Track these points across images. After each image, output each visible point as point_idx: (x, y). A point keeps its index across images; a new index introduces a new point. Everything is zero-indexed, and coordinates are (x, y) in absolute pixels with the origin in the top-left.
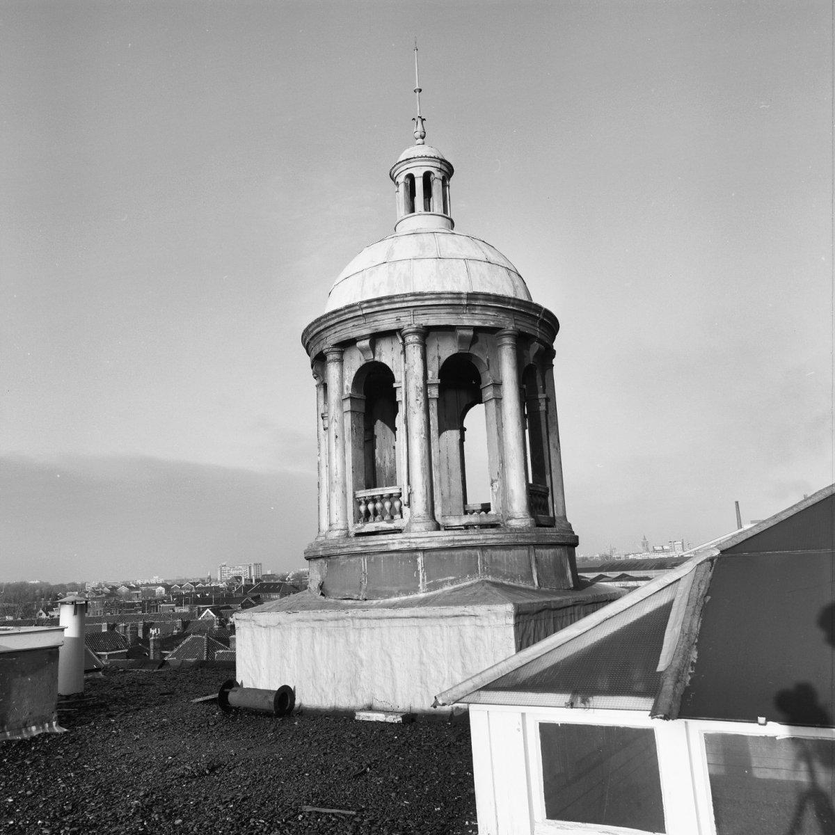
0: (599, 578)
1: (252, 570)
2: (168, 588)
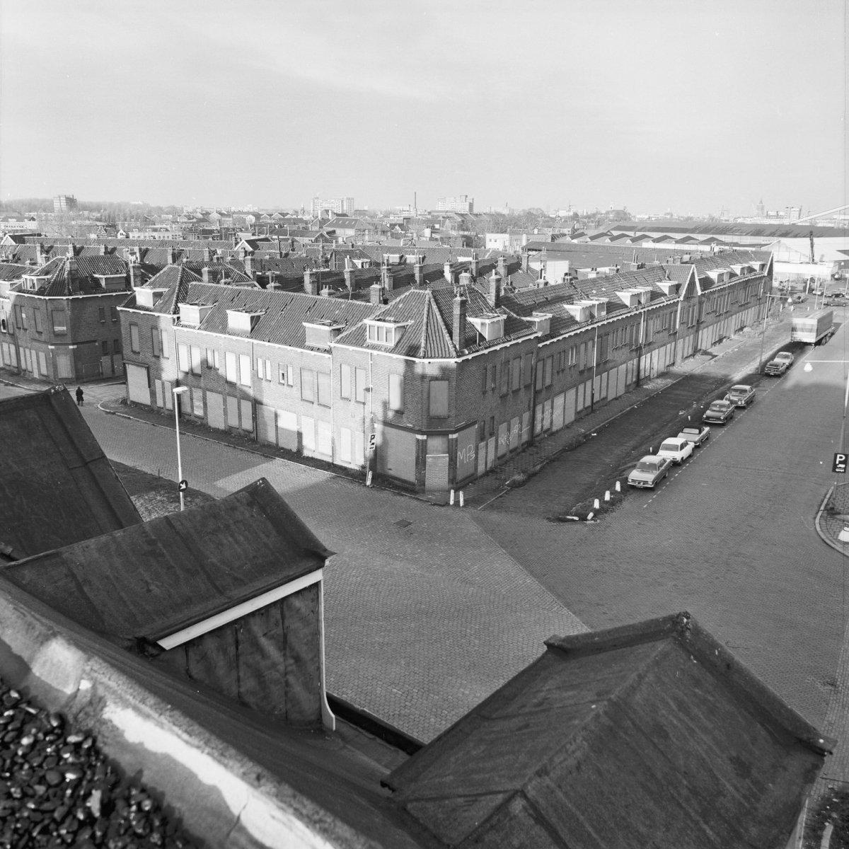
0: (644, 237)
1: (345, 204)
2: (258, 216)
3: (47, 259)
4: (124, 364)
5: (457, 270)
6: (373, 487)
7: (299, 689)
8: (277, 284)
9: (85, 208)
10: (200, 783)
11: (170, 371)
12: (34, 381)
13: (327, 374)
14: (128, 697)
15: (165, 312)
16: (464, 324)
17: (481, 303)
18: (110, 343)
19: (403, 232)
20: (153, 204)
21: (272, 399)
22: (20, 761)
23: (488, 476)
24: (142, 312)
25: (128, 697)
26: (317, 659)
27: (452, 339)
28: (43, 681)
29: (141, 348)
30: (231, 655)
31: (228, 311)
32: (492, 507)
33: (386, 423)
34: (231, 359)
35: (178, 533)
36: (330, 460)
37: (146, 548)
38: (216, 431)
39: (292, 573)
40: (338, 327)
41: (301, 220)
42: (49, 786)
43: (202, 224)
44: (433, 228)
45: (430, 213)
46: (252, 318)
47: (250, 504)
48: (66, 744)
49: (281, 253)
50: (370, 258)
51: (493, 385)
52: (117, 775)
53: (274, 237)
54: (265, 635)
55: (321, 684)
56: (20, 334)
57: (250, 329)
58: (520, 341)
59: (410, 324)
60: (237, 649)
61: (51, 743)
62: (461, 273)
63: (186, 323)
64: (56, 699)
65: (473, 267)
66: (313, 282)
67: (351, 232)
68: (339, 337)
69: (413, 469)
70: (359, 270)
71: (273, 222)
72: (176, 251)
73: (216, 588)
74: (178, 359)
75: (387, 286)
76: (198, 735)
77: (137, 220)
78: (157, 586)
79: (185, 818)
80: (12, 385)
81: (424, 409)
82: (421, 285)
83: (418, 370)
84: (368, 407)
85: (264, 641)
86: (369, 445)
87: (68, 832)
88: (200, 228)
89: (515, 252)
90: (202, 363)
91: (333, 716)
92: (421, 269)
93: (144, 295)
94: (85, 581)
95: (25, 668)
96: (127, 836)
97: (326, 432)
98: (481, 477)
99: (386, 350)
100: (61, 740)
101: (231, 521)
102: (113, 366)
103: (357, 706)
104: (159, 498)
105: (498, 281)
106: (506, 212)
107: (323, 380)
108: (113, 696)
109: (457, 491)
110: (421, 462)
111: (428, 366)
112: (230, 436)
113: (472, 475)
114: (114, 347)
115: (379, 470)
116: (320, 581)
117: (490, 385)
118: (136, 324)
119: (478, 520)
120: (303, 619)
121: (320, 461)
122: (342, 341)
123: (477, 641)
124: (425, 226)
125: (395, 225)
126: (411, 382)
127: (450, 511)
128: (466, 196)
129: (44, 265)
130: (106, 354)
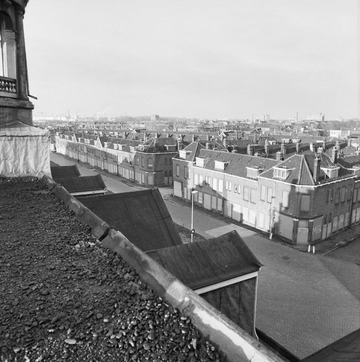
2: (228, 122)
3: (148, 139)
4: (173, 180)
5: (316, 147)
6: (273, 240)
7: (244, 322)
8: (236, 151)
9: (162, 119)
10: (234, 344)
11: (191, 185)
12: (139, 185)
13: (255, 189)
14: (204, 306)
15: (190, 161)
16: (319, 170)
17: (327, 161)
18: (168, 172)
19: (291, 129)
20: (187, 118)
21: (231, 199)
22: (165, 323)
23: (327, 240)
24: (181, 160)
25: (204, 306)
26: (252, 310)
27: (313, 177)
28: (170, 296)
29: (180, 174)
30: (218, 302)
31: (215, 161)
32: (328, 255)
33: (281, 213)
34: (215, 181)
35: (200, 249)
36: (254, 226)
37: (188, 253)
38: (207, 210)
39: (245, 271)
40: (261, 169)
41: (247, 124)
42: (176, 334)
43: (206, 125)
44: (305, 127)
45: (304, 121)
46: (225, 164)
47: (229, 241)
48: (180, 320)
49: (238, 138)
50: (276, 140)
51: (332, 199)
52: (200, 335)
53: (235, 131)
54: (232, 296)
55: (254, 322)
56: (136, 167)
57: (223, 169)
58: (346, 179)
59: (294, 169)
60: (221, 300)
61: (175, 318)
62: (318, 147)
63: (198, 165)
64: (175, 303)
65: (324, 145)
66: (251, 150)
67: (268, 129)
68: (261, 174)
69: (291, 234)
70: (271, 146)
71: (235, 125)
72: (196, 136)
73: (215, 273)
74: (194, 180)
75: (283, 153)
76: (233, 325)
77: (181, 124)
78: (192, 269)
79: (228, 356)
80: (132, 186)
81: (298, 208)
82: (299, 152)
83: (297, 190)
84: (273, 205)
85: (231, 298)
86: (272, 221)
87: (185, 352)
88: (205, 127)
89: (344, 138)
90: (203, 182)
91: (258, 337)
92: (299, 145)
93: (182, 154)
94: (165, 263)
95: (165, 291)
96: (207, 358)
97: (253, 214)
98: (324, 241)
99: (282, 180)
100: (178, 318)
101: (221, 247)
102: (168, 181)
103: (267, 335)
104: (183, 235)
105: (336, 152)
106: (340, 120)
107: (253, 192)
108: (198, 305)
109: (312, 246)
110: (295, 231)
111: (302, 188)
112: (212, 213)
113: (320, 239)
114: (170, 174)
115: (276, 233)
116: (256, 277)
117: (330, 198)
118: (178, 165)
119: (321, 260)
120: (248, 292)
121: (250, 226)
122: (263, 176)
123: (319, 318)
124: (301, 126)
125: (288, 126)
126: (293, 195)
127: (308, 255)
128: (321, 114)
129: (147, 141)
130: (166, 176)
